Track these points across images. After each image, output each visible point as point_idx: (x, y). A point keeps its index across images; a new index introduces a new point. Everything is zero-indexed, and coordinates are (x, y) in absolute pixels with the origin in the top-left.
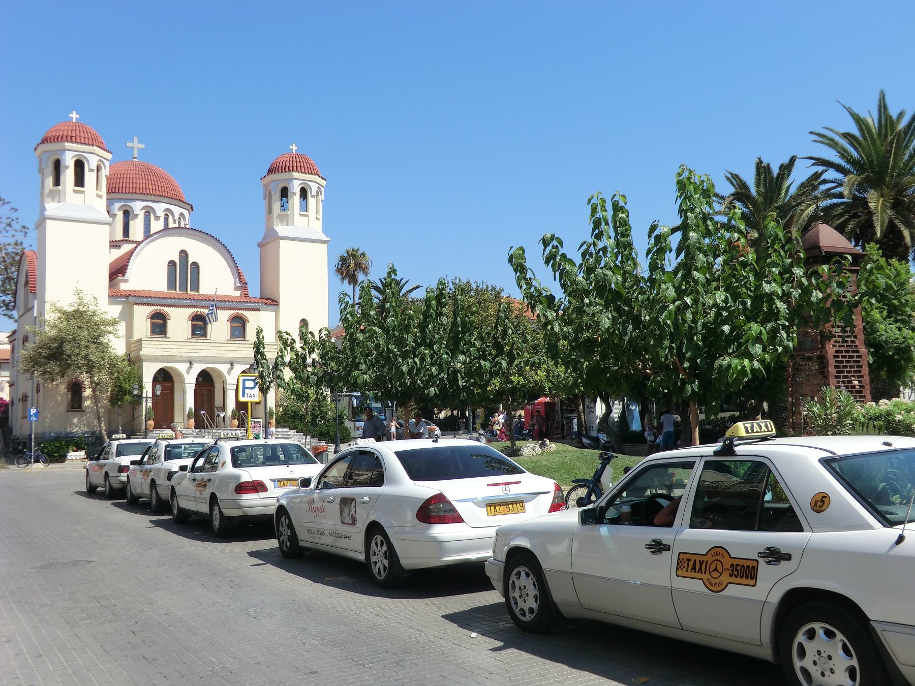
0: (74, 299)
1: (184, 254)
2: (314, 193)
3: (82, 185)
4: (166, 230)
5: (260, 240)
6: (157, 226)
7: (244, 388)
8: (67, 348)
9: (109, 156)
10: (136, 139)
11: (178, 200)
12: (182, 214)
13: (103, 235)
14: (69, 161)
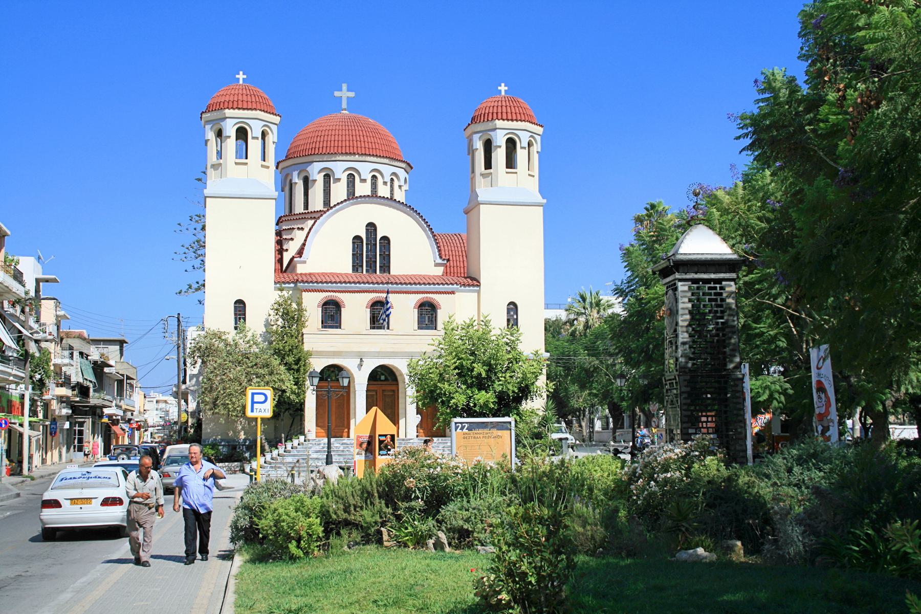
1: (371, 228)
4: (373, 196)
5: (465, 205)
7: (253, 402)
9: (277, 119)
10: (344, 87)
12: (394, 174)
14: (500, 140)
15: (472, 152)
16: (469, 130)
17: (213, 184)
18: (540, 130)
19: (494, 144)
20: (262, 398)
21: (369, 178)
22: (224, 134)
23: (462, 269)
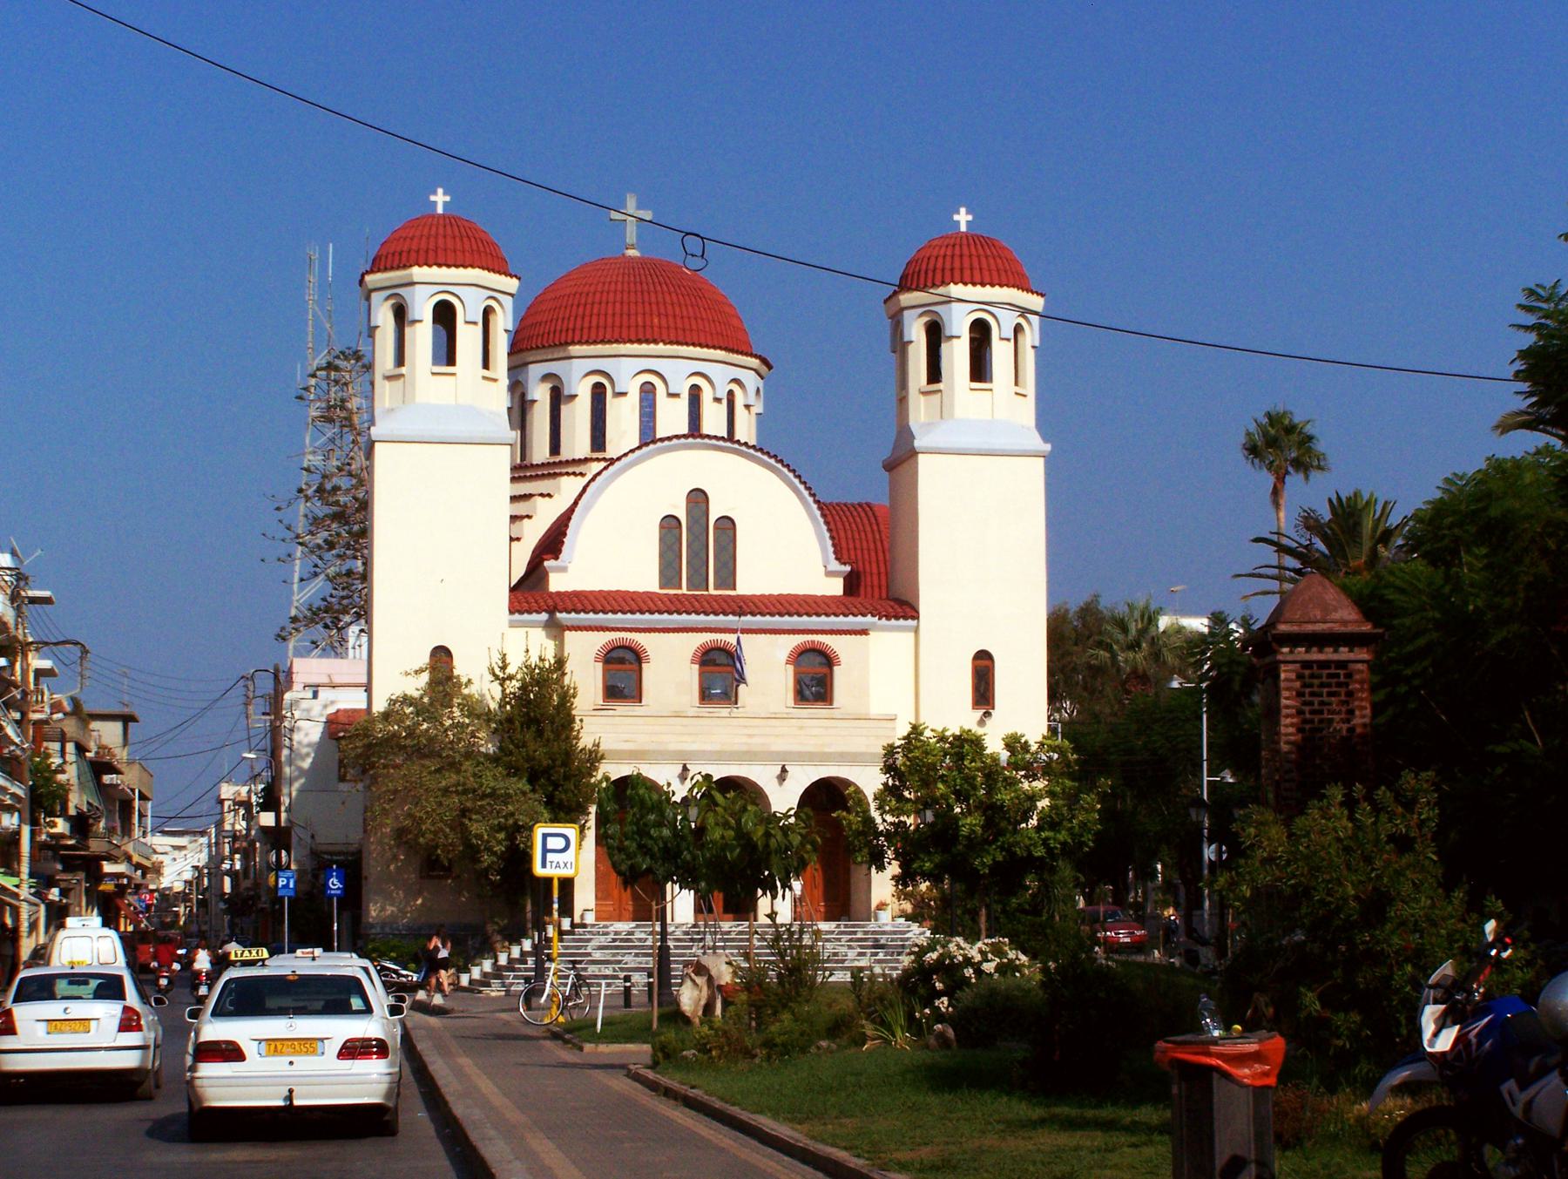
1: (698, 499)
3: (451, 361)
5: (886, 453)
7: (545, 851)
9: (512, 284)
13: (502, 459)
14: (959, 322)
15: (900, 346)
20: (560, 843)
23: (877, 578)
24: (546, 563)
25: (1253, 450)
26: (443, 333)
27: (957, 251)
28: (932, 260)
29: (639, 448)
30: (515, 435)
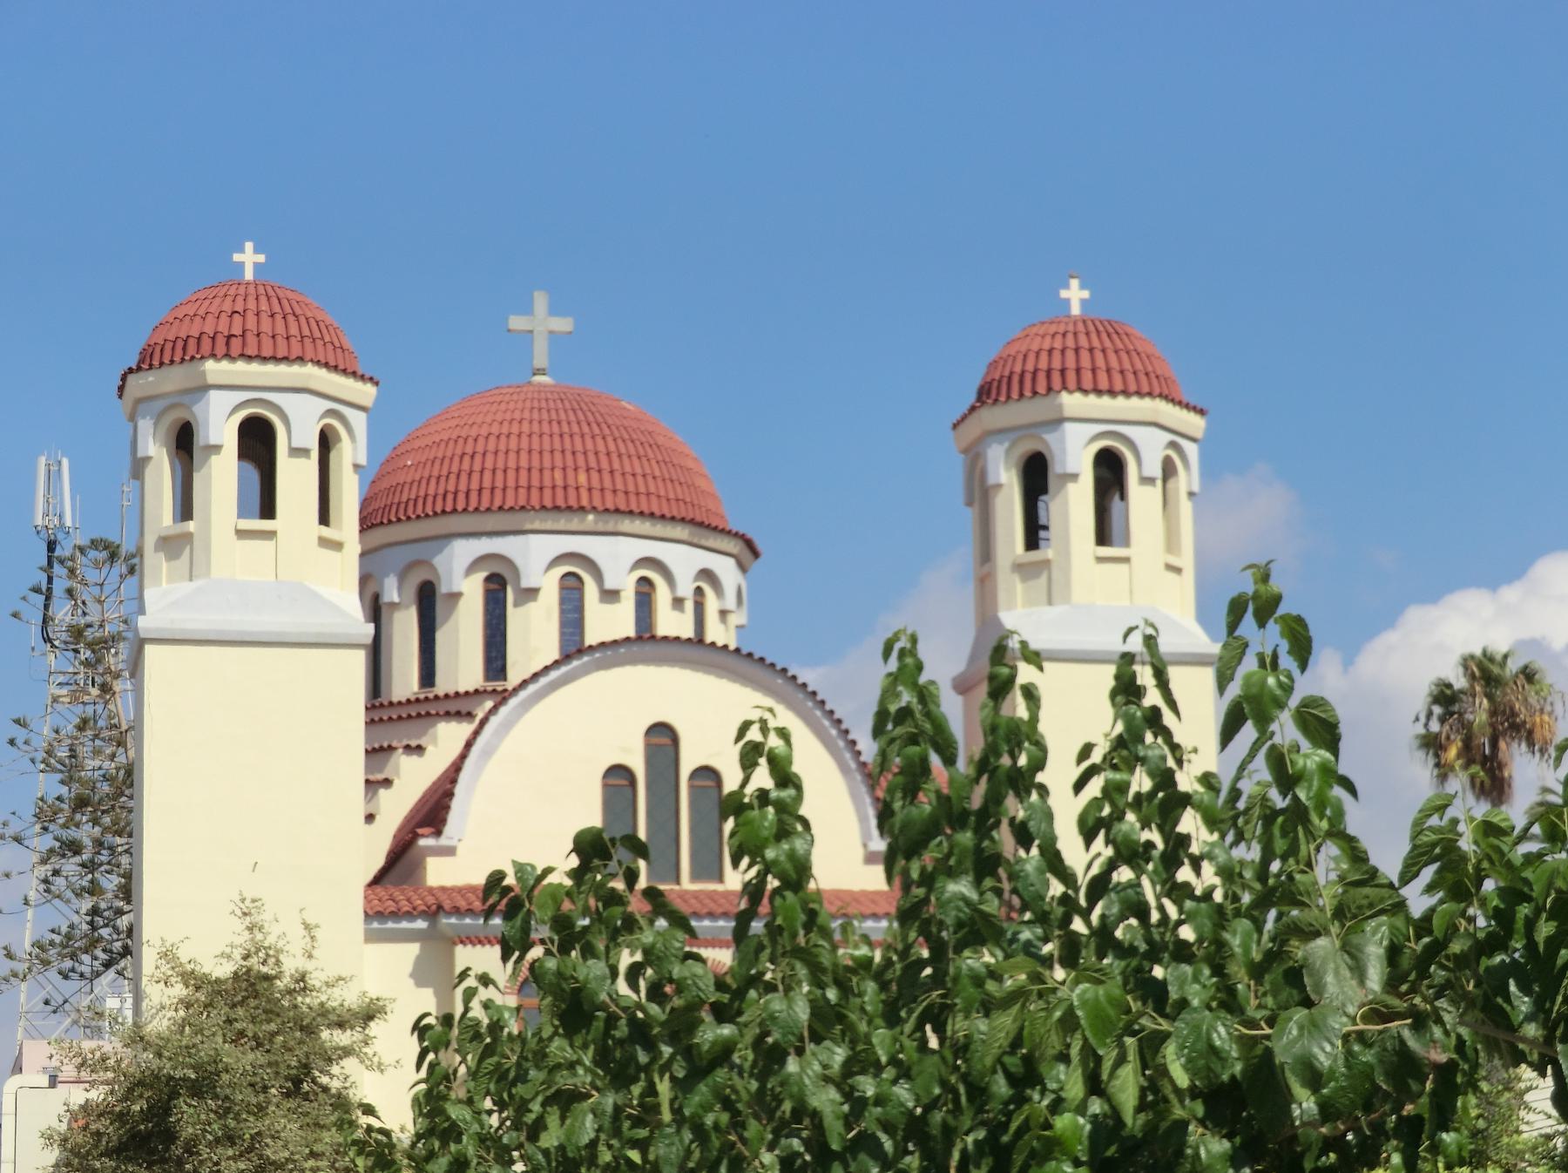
0: (233, 934)
1: (663, 738)
2: (1154, 469)
3: (268, 509)
4: (645, 641)
6: (608, 621)
8: (190, 1117)
9: (365, 393)
11: (702, 525)
12: (706, 574)
14: (1075, 454)
15: (980, 494)
16: (973, 429)
17: (165, 598)
18: (1194, 423)
19: (1056, 468)
21: (627, 585)
22: (199, 440)
24: (422, 842)
25: (1526, 667)
26: (254, 476)
27: (1070, 342)
28: (1031, 357)
29: (556, 664)
30: (370, 629)
